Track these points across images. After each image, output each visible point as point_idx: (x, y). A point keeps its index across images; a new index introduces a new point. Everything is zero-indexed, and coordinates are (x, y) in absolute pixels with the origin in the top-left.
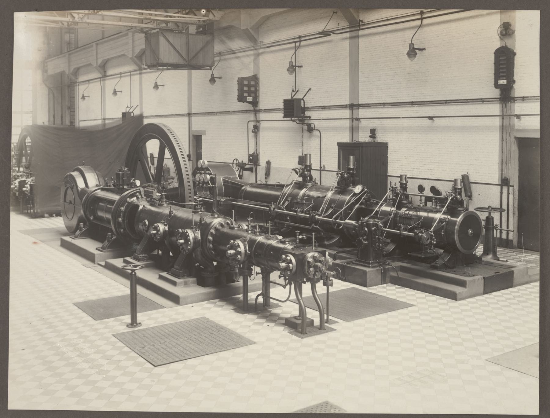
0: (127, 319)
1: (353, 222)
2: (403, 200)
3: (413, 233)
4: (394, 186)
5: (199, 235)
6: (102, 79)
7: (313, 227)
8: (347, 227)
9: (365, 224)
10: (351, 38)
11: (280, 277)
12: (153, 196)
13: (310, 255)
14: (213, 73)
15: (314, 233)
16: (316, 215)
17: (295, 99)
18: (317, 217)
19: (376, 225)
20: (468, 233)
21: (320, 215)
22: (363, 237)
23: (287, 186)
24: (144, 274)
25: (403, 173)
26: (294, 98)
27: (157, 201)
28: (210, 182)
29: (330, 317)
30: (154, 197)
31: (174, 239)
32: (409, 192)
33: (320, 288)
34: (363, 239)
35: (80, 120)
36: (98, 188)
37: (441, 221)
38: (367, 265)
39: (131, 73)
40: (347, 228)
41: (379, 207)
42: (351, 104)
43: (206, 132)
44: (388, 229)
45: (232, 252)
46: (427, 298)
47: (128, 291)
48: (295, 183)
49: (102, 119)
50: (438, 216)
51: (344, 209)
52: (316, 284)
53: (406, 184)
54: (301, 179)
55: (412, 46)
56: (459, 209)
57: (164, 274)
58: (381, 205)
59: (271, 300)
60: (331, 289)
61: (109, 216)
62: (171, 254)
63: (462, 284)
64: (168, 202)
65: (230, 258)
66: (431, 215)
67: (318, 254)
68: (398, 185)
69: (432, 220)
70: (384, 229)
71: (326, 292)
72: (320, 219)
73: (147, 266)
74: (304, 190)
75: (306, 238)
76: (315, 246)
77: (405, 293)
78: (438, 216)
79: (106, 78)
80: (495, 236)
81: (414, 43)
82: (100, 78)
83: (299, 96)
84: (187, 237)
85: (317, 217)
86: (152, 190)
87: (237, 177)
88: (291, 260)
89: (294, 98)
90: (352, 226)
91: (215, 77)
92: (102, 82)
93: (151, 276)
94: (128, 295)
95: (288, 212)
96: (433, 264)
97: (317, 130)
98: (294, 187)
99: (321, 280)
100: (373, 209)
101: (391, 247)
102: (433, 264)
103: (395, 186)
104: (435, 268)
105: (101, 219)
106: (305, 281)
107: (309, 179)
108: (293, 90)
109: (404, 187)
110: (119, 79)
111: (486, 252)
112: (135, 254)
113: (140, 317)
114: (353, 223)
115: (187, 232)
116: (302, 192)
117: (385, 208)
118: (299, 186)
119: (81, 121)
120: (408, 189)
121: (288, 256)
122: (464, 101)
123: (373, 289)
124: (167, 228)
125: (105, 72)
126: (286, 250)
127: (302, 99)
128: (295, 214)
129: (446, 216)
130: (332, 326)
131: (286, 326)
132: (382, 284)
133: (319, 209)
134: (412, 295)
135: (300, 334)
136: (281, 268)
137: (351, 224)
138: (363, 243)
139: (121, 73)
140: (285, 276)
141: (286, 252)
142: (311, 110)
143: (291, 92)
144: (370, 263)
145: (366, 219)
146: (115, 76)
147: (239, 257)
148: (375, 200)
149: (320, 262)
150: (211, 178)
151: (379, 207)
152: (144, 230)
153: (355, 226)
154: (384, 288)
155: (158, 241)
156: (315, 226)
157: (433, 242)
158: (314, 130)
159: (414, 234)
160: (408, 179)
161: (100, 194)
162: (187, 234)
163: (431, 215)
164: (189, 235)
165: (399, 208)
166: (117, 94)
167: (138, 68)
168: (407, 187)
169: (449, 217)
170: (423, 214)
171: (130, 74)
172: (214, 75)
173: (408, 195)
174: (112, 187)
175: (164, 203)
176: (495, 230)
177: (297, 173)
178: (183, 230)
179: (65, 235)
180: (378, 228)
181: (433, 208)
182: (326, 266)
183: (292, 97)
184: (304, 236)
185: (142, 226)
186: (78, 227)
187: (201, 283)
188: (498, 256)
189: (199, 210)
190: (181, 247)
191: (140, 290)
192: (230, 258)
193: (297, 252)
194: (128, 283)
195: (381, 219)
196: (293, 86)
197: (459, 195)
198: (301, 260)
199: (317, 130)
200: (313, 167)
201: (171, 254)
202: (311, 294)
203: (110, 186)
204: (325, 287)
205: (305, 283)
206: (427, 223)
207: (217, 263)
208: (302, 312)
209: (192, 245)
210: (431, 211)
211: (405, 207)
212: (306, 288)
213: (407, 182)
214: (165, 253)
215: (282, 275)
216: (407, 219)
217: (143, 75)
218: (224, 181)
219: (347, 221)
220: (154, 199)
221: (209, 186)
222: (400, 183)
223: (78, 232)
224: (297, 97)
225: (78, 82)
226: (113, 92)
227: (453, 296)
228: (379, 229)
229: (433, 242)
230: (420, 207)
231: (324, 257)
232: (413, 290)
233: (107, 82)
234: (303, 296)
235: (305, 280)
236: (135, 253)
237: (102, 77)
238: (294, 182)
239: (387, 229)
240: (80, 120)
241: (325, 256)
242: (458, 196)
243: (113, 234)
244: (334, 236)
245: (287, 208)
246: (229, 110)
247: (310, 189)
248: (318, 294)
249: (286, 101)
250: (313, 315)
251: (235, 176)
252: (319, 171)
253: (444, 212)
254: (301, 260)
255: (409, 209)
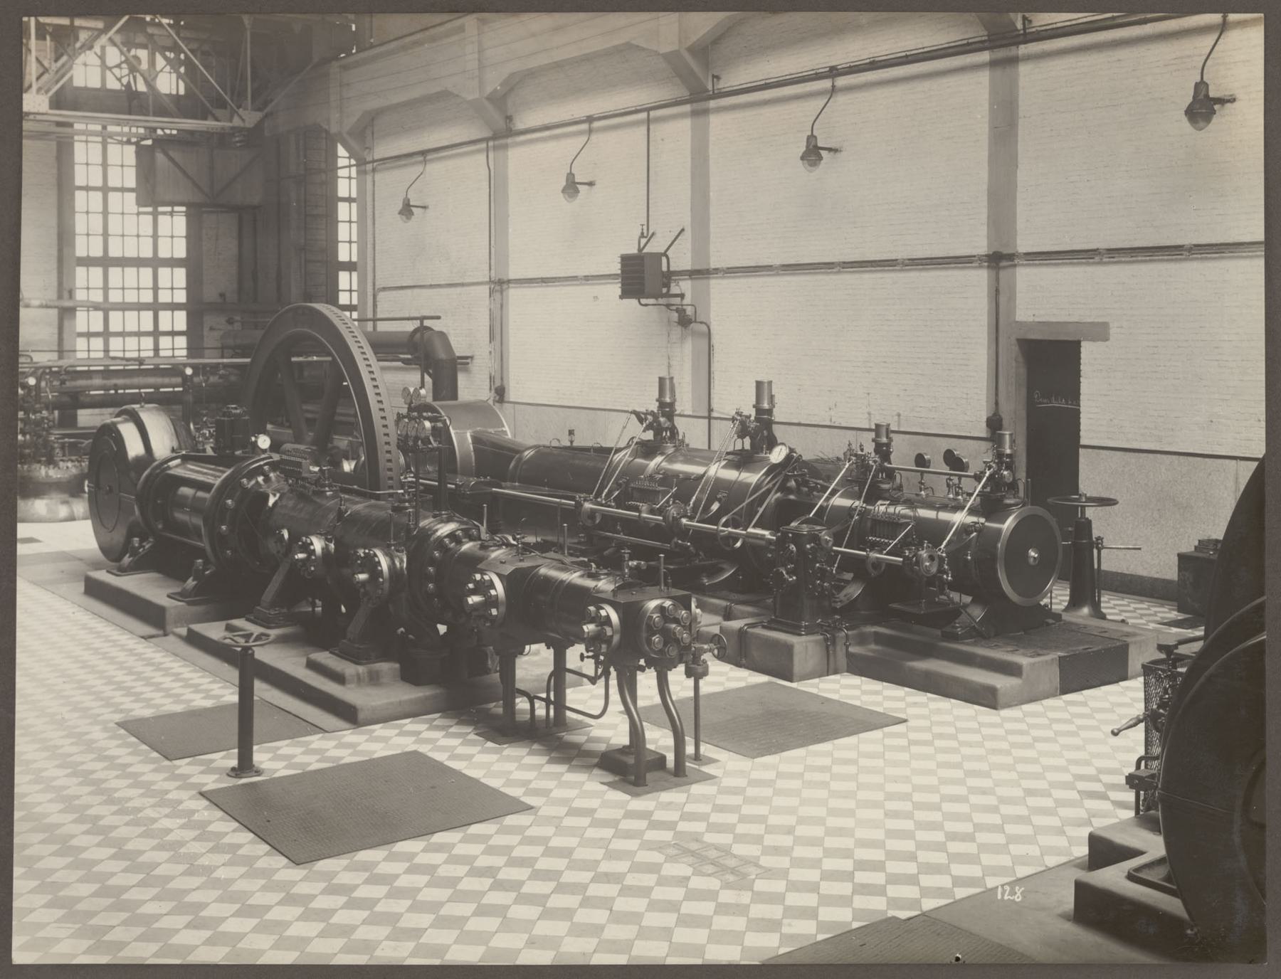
0: (230, 760)
1: (766, 533)
2: (881, 482)
3: (900, 557)
4: (860, 453)
5: (402, 561)
6: (491, 144)
7: (676, 544)
8: (753, 547)
9: (790, 535)
10: (993, 64)
11: (582, 657)
12: (300, 473)
13: (652, 604)
14: (573, 172)
15: (662, 555)
16: (681, 518)
17: (647, 253)
18: (684, 521)
19: (815, 538)
20: (1027, 556)
21: (691, 518)
22: (784, 566)
23: (618, 450)
24: (266, 655)
25: (878, 419)
26: (645, 251)
27: (312, 484)
28: (431, 438)
29: (705, 749)
30: (304, 475)
31: (346, 571)
32: (896, 462)
33: (679, 682)
34: (786, 569)
35: (379, 284)
36: (174, 455)
37: (965, 529)
38: (795, 631)
39: (648, 115)
40: (755, 548)
41: (828, 499)
42: (994, 253)
43: (1112, 331)
44: (845, 548)
45: (474, 599)
46: (956, 712)
47: (232, 697)
48: (637, 443)
49: (491, 281)
50: (959, 518)
51: (747, 505)
52: (669, 672)
53: (888, 445)
54: (649, 435)
55: (406, 202)
56: (1008, 501)
57: (324, 657)
58: (834, 493)
59: (569, 713)
60: (707, 686)
61: (198, 521)
62: (343, 609)
63: (1011, 670)
64: (336, 486)
65: (475, 613)
66: (943, 516)
67: (670, 603)
68: (869, 448)
69: (947, 526)
70: (835, 548)
71: (691, 694)
72: (691, 525)
73: (283, 640)
74: (659, 459)
75: (645, 568)
76: (666, 584)
77: (1006, 731)
78: (959, 518)
79: (509, 140)
80: (1096, 566)
81: (1208, 82)
82: (486, 140)
83: (655, 247)
84: (376, 567)
85: (684, 521)
86: (299, 460)
87: (506, 431)
88: (608, 617)
89: (645, 251)
90: (763, 543)
91: (577, 181)
92: (491, 155)
93: (290, 662)
94: (235, 704)
95: (620, 511)
96: (948, 629)
97: (701, 323)
98: (635, 454)
99: (681, 662)
100: (813, 502)
101: (855, 591)
102: (948, 629)
103: (862, 450)
104: (955, 638)
105: (183, 529)
106: (644, 664)
107: (668, 434)
108: (642, 233)
109: (883, 451)
110: (584, 139)
111: (1074, 603)
112: (258, 608)
113: (260, 757)
114: (764, 535)
115: (375, 555)
116: (653, 464)
117: (838, 501)
118: (648, 450)
119: (384, 289)
120: (892, 457)
121: (603, 608)
122: (747, 270)
123: (813, 686)
124: (332, 546)
125: (509, 119)
126: (599, 595)
127: (665, 254)
128: (635, 516)
129: (974, 519)
130: (705, 769)
131: (535, 746)
132: (828, 675)
133: (690, 501)
134: (877, 693)
135: (631, 787)
136: (586, 636)
137: (762, 537)
138: (786, 580)
139: (590, 119)
140: (595, 657)
141: (599, 601)
142: (1105, 260)
143: (638, 237)
144: (801, 627)
145: (794, 524)
146: (529, 137)
147: (494, 612)
148: (818, 481)
149: (677, 621)
150: (434, 428)
151: (828, 499)
152: (278, 552)
153: (769, 541)
154: (834, 681)
155: (309, 577)
156: (680, 542)
157: (945, 576)
158: (695, 322)
159: (901, 559)
160: (892, 435)
161: (178, 469)
162: (377, 559)
163: (943, 516)
164: (379, 562)
165: (872, 498)
166: (412, 214)
167: (683, 93)
168: (891, 452)
169: (982, 520)
170: (924, 513)
171: (643, 115)
172: (816, 137)
173: (893, 470)
174: (210, 452)
175: (327, 489)
176: (1095, 551)
177: (641, 421)
178: (367, 551)
179: (97, 566)
180: (820, 544)
181: (949, 499)
182: (690, 630)
183: (640, 250)
184: (642, 563)
185: (276, 542)
186: (126, 548)
187: (410, 676)
188: (1104, 611)
189: (407, 504)
190: (362, 590)
191: (262, 690)
192: (475, 613)
193: (621, 599)
194: (234, 674)
195: (829, 525)
196: (643, 225)
197: (1007, 469)
198: (631, 614)
199: (701, 323)
200: (679, 408)
201: (343, 609)
202: (658, 700)
203: (204, 450)
204: (691, 682)
205: (642, 669)
206: (934, 532)
207: (448, 629)
208: (636, 733)
209: (386, 586)
210: (944, 507)
211: (885, 499)
212: (647, 682)
213: (890, 440)
214: (331, 608)
215: (590, 654)
216: (892, 525)
217: (714, 120)
218: (476, 440)
219: (750, 530)
220: (304, 479)
221: (430, 446)
222: (874, 444)
223: (127, 560)
224: (651, 248)
225: (374, 161)
226: (564, 183)
227: (987, 698)
228: (822, 549)
229: (945, 576)
230: (920, 498)
231: (686, 609)
232: (924, 693)
233: (512, 153)
234: (640, 703)
235: (642, 662)
236: (259, 605)
237: (494, 138)
238: (635, 441)
239: (843, 549)
240: (379, 284)
241: (688, 608)
242: (1005, 473)
243: (207, 563)
244: (725, 566)
245: (620, 503)
246: (1179, 242)
247: (670, 459)
248: (674, 698)
249: (626, 260)
250: (659, 739)
251: (500, 429)
252: (707, 420)
253: (969, 509)
254: (631, 614)
255: (895, 502)
